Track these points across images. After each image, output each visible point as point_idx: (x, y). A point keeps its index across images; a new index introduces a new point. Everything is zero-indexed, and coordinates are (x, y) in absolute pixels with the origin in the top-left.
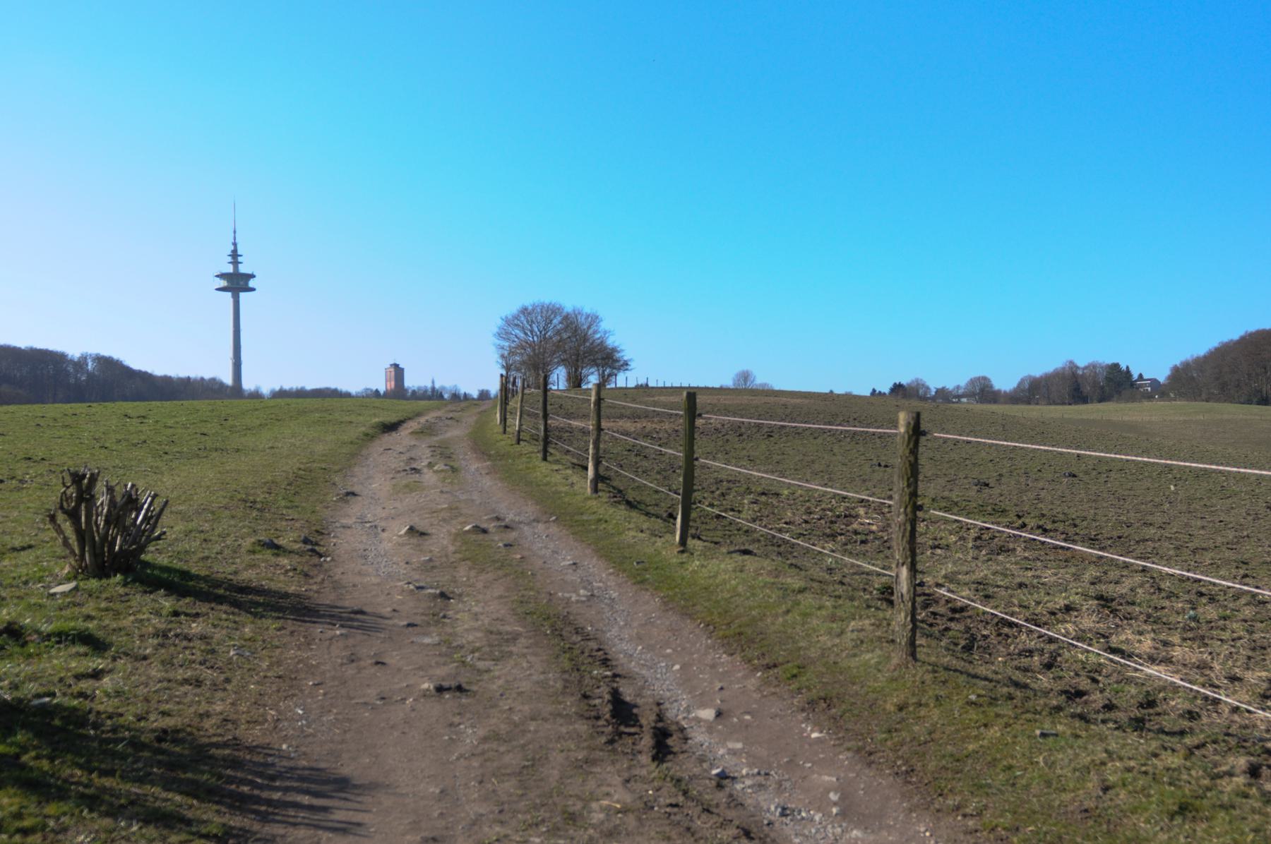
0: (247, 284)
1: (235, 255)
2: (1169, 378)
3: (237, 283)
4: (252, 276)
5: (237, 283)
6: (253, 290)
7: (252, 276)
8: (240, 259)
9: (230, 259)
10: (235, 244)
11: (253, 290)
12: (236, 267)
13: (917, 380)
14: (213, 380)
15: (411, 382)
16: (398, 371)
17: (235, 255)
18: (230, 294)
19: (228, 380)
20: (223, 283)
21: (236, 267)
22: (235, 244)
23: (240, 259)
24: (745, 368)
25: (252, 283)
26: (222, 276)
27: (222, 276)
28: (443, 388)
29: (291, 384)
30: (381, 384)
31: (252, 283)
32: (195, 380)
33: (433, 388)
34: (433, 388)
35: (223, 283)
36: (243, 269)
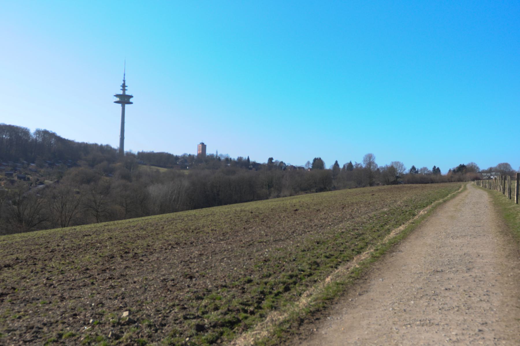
0: (129, 100)
1: (124, 86)
2: (212, 156)
3: (124, 99)
4: (132, 97)
5: (124, 99)
6: (132, 103)
7: (132, 97)
8: (126, 88)
9: (121, 88)
10: (124, 81)
11: (132, 103)
12: (124, 90)
13: (472, 163)
14: (107, 146)
15: (209, 151)
16: (203, 146)
17: (124, 86)
18: (120, 105)
19: (115, 145)
20: (118, 99)
21: (124, 90)
22: (124, 81)
23: (126, 88)
24: (370, 152)
25: (131, 100)
26: (117, 96)
27: (117, 96)
28: (221, 155)
29: (147, 149)
30: (194, 151)
31: (131, 100)
32: (105, 146)
33: (217, 156)
34: (217, 156)
35: (118, 99)
36: (127, 93)
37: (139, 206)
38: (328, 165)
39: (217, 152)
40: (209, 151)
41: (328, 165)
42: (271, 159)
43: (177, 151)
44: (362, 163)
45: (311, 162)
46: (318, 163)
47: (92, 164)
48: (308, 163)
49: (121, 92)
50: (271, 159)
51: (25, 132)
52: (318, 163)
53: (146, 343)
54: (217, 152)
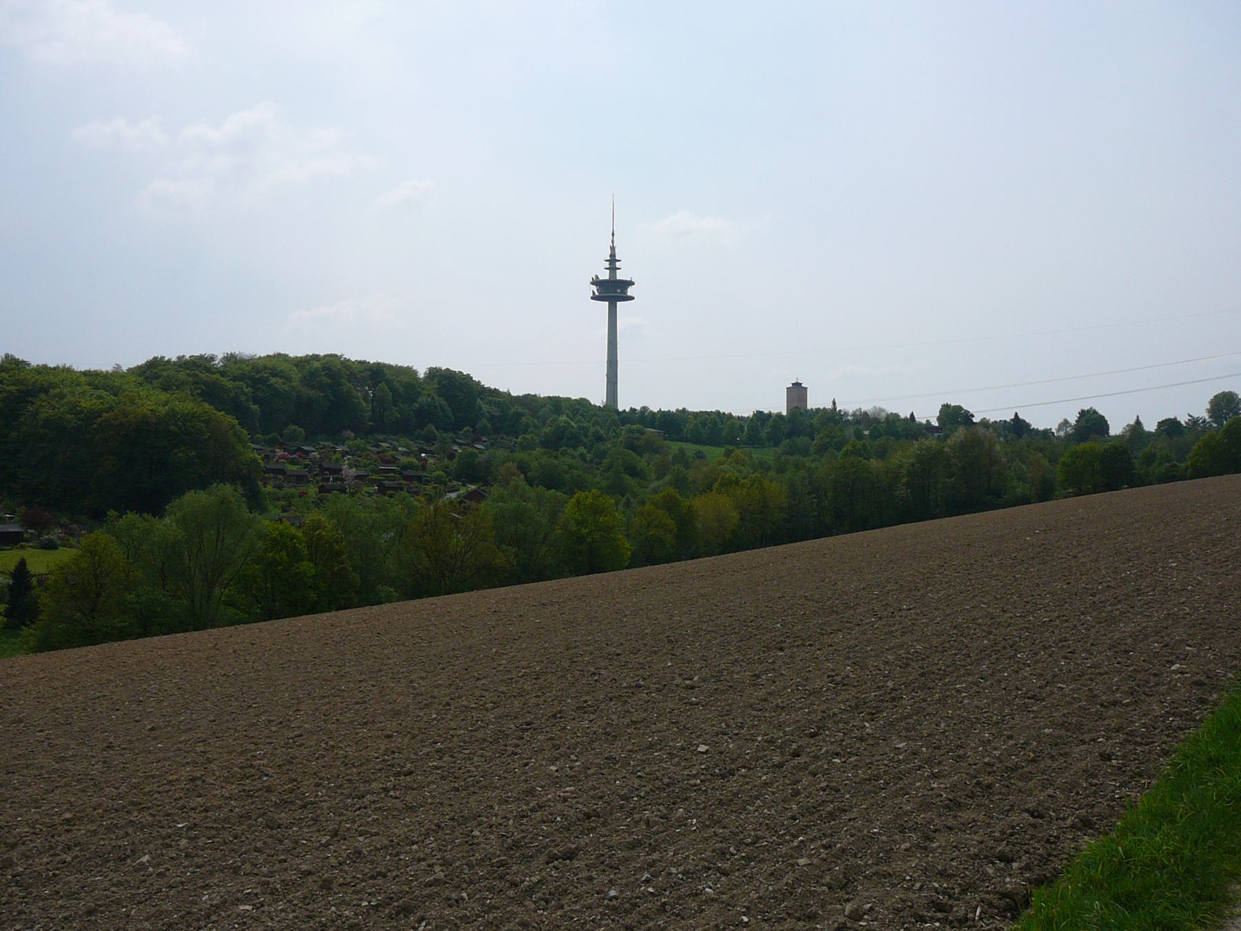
1: (613, 260)
3: (612, 291)
4: (631, 283)
5: (612, 291)
6: (632, 298)
7: (631, 283)
9: (607, 265)
10: (613, 248)
11: (632, 298)
17: (613, 260)
19: (598, 398)
22: (613, 248)
23: (618, 265)
31: (630, 291)
36: (620, 276)
37: (679, 541)
38: (1116, 428)
39: (834, 403)
40: (816, 400)
41: (1116, 428)
42: (797, 392)
43: (742, 408)
44: (1206, 416)
45: (1073, 420)
46: (1092, 423)
47: (556, 441)
48: (1066, 422)
49: (605, 276)
50: (797, 392)
51: (409, 372)
52: (1092, 423)
53: (665, 928)
54: (834, 403)
